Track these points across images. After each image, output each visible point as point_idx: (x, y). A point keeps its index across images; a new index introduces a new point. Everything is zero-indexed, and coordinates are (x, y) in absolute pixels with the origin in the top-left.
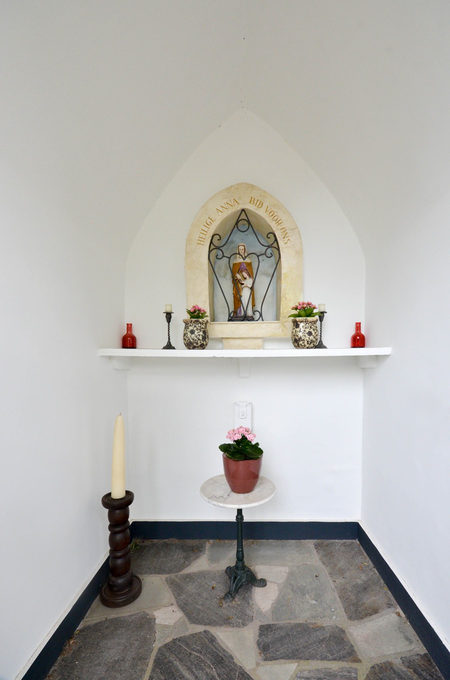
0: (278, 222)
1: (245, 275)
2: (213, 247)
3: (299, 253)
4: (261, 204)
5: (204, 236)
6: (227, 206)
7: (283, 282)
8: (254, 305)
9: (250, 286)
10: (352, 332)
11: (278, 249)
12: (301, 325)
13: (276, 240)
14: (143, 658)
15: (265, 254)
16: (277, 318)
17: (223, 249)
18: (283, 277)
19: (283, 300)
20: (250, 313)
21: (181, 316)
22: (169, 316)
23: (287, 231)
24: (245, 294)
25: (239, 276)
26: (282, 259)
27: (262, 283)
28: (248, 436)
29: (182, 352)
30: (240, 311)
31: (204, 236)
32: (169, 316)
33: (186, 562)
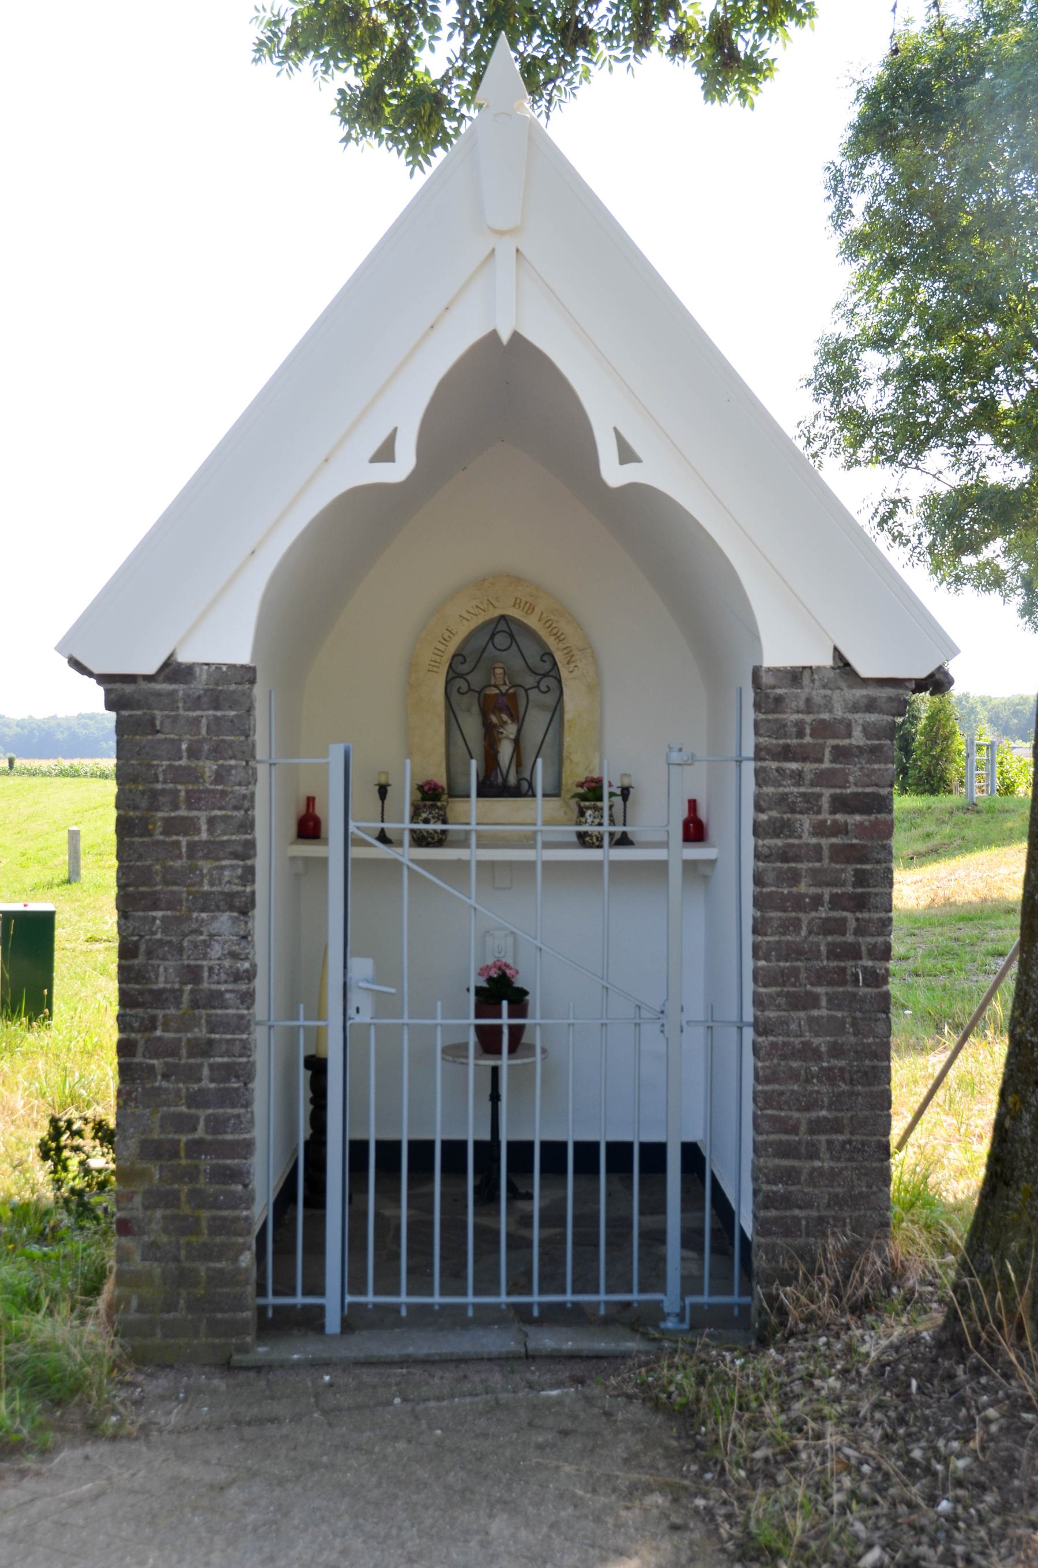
0: (559, 637)
1: (505, 717)
2: (453, 675)
3: (595, 688)
4: (532, 609)
5: (438, 659)
6: (477, 611)
7: (566, 733)
8: (519, 765)
9: (512, 737)
10: (681, 813)
11: (560, 681)
12: (589, 813)
13: (555, 664)
14: (768, 721)
15: (538, 687)
16: (554, 792)
17: (468, 677)
18: (566, 727)
19: (567, 763)
20: (512, 780)
21: (404, 796)
22: (383, 791)
23: (575, 652)
24: (505, 751)
25: (494, 719)
26: (566, 697)
27: (536, 722)
28: (508, 972)
29: (407, 854)
30: (496, 777)
31: (438, 659)
32: (383, 791)
33: (227, 879)
